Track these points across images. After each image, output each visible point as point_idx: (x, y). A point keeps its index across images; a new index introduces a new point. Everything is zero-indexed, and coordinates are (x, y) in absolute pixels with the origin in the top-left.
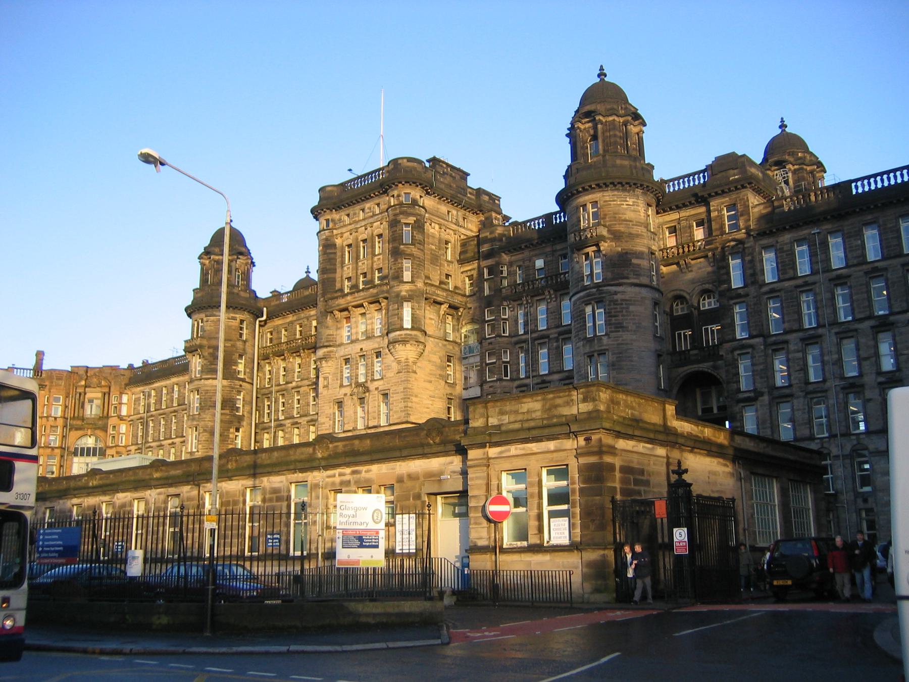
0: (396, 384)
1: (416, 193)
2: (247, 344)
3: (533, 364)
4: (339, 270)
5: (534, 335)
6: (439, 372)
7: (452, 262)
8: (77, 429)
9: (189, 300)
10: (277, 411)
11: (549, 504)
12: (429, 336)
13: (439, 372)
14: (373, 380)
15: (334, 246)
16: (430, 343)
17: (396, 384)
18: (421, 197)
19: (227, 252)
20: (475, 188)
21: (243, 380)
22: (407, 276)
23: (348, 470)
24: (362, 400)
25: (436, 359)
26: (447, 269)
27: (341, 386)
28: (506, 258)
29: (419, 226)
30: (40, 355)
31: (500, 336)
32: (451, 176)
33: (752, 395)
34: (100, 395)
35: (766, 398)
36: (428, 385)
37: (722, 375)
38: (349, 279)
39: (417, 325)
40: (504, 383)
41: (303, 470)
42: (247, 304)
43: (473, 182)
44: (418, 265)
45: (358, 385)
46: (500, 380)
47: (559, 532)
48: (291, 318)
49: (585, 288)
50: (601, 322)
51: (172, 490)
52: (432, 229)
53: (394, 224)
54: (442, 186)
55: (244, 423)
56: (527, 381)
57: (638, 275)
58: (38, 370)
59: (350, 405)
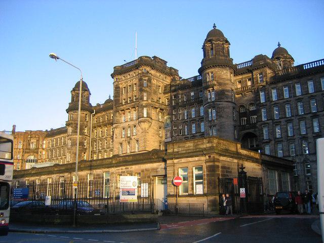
1: (148, 69)
3: (190, 130)
4: (121, 96)
9: (67, 107)
10: (99, 146)
16: (153, 122)
19: (81, 90)
21: (87, 135)
22: (145, 98)
23: (124, 168)
25: (155, 128)
26: (159, 96)
28: (180, 92)
29: (149, 81)
30: (14, 127)
33: (268, 141)
34: (35, 141)
35: (273, 142)
37: (257, 134)
41: (108, 168)
42: (88, 108)
43: (168, 65)
44: (149, 94)
45: (128, 137)
46: (178, 135)
47: (199, 189)
48: (104, 113)
49: (209, 103)
50: (214, 115)
51: (61, 175)
52: (154, 82)
53: (140, 80)
56: (188, 136)
57: (227, 98)
58: (13, 132)
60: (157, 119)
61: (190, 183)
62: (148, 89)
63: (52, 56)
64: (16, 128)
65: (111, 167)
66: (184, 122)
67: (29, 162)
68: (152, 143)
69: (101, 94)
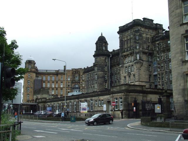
0: (136, 72)
1: (139, 28)
2: (107, 63)
4: (124, 46)
5: (168, 59)
6: (147, 69)
7: (150, 43)
8: (74, 83)
9: (94, 53)
10: (115, 78)
11: (121, 103)
12: (144, 61)
13: (147, 69)
14: (132, 72)
15: (123, 40)
16: (144, 63)
17: (136, 72)
18: (141, 28)
19: (102, 42)
20: (94, 58)
21: (107, 72)
22: (138, 48)
23: (97, 97)
24: (129, 76)
25: (146, 66)
27: (125, 73)
28: (161, 41)
29: (140, 35)
30: (65, 67)
31: (161, 60)
32: (149, 21)
34: (78, 75)
36: (144, 72)
38: (126, 48)
39: (140, 59)
40: (162, 71)
41: (92, 97)
42: (107, 54)
43: (155, 22)
45: (129, 73)
46: (161, 70)
51: (75, 100)
52: (144, 35)
54: (146, 25)
55: (107, 81)
56: (167, 70)
58: (65, 70)
59: (127, 78)
60: (147, 60)
61: (118, 104)
62: (139, 41)
63: (53, 59)
64: (66, 67)
65: (93, 97)
66: (165, 61)
67: (75, 89)
68: (96, 88)
69: (113, 45)
